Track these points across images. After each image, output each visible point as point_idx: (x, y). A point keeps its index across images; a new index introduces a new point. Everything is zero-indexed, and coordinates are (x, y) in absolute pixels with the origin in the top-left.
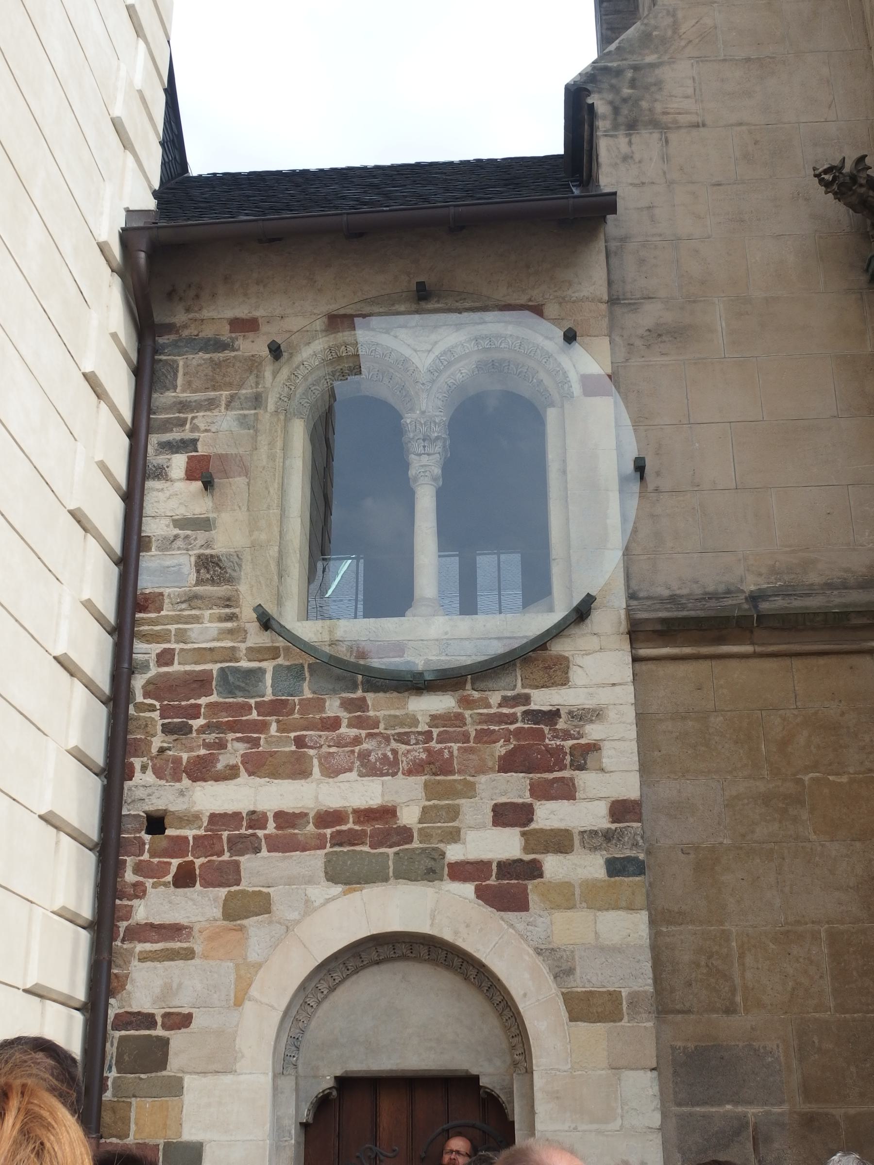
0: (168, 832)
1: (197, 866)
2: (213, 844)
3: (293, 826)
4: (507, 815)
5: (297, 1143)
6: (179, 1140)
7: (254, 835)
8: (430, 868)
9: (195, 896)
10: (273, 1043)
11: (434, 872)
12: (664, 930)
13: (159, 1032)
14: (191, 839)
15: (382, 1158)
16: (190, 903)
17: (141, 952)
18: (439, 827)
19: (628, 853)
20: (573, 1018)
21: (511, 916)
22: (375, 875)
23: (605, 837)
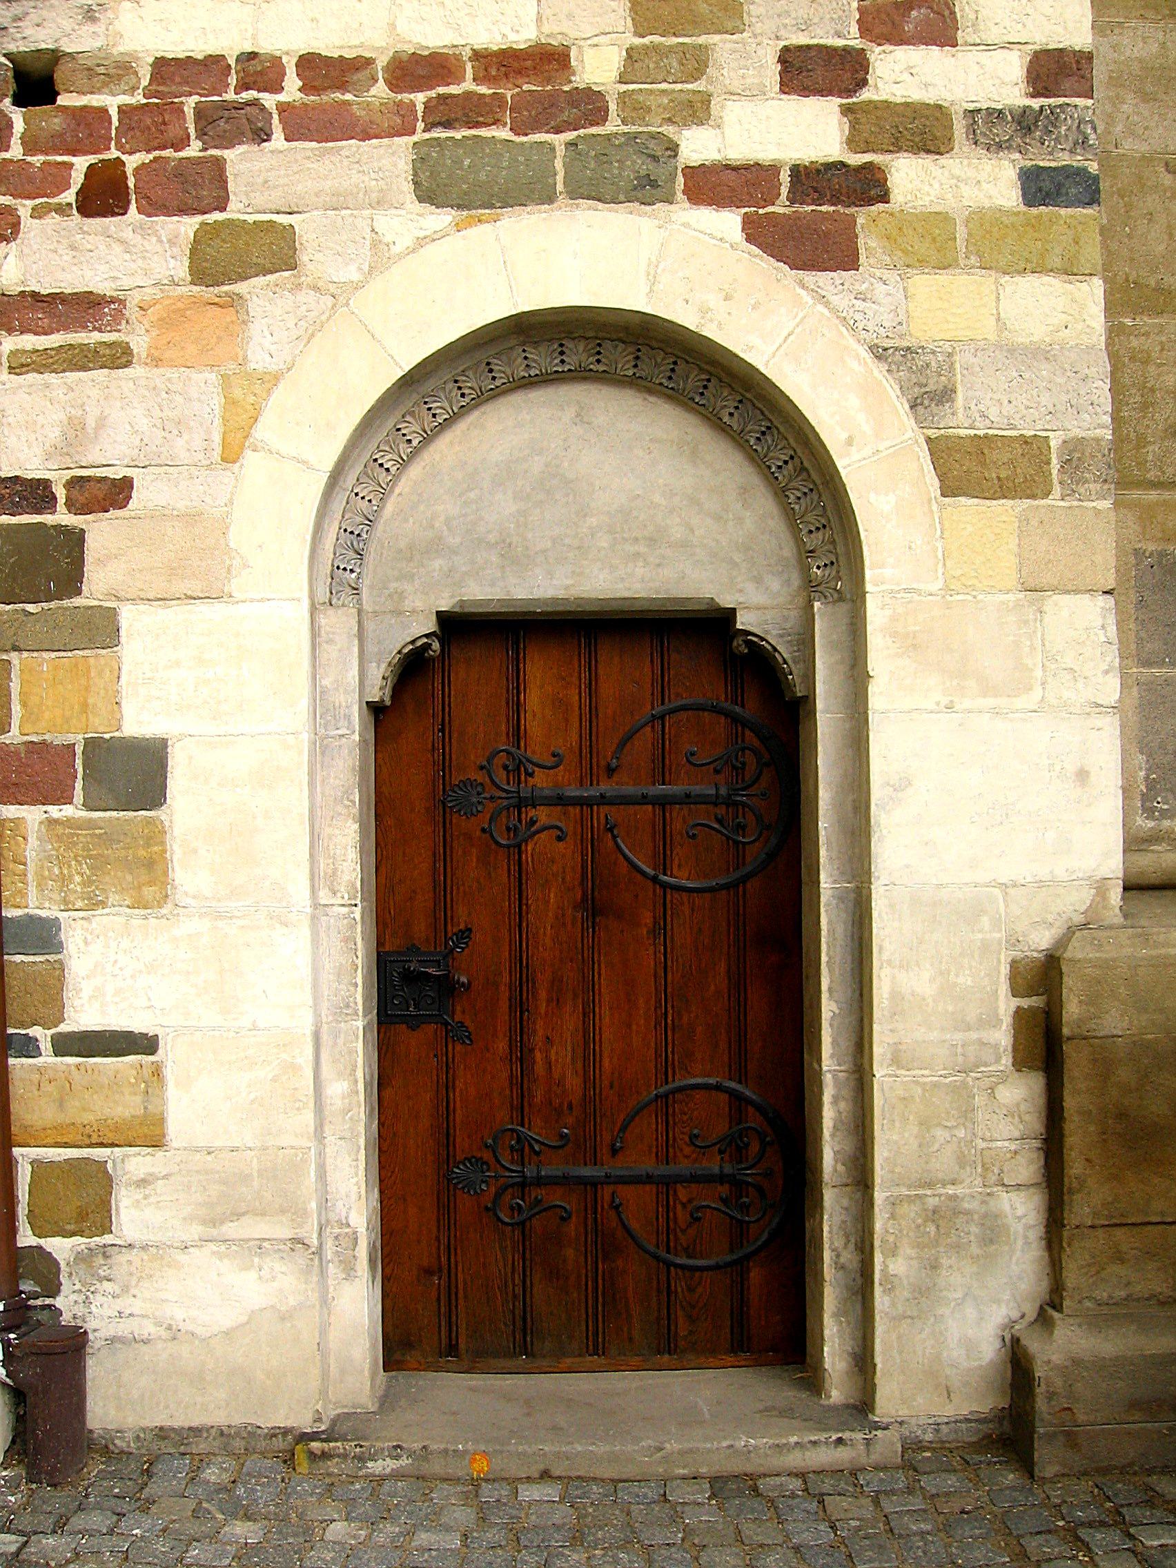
0: (62, 100)
1: (129, 170)
2: (164, 123)
3: (343, 87)
4: (805, 71)
5: (363, 741)
6: (117, 734)
7: (254, 103)
8: (640, 175)
9: (128, 234)
10: (309, 538)
11: (654, 184)
12: (1128, 322)
13: (62, 517)
14: (114, 113)
15: (530, 768)
16: (117, 248)
17: (13, 353)
18: (664, 91)
19: (1065, 159)
20: (948, 491)
21: (823, 279)
22: (526, 190)
23: (1019, 123)
